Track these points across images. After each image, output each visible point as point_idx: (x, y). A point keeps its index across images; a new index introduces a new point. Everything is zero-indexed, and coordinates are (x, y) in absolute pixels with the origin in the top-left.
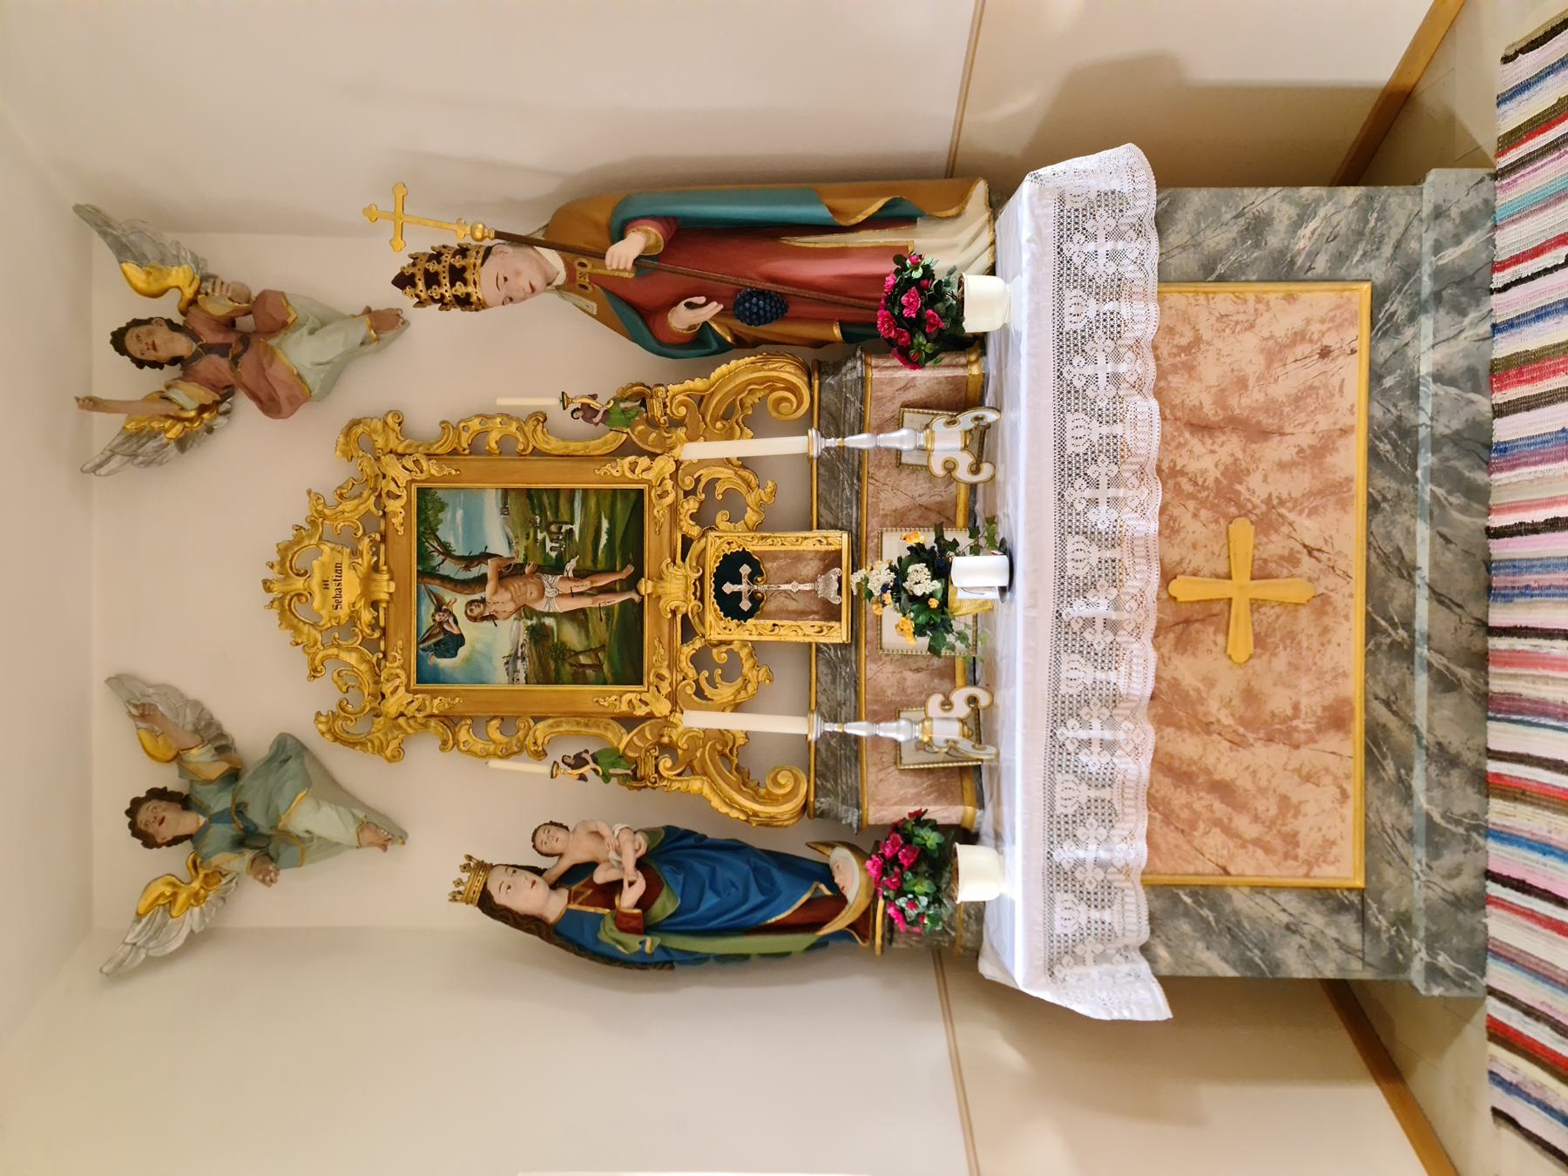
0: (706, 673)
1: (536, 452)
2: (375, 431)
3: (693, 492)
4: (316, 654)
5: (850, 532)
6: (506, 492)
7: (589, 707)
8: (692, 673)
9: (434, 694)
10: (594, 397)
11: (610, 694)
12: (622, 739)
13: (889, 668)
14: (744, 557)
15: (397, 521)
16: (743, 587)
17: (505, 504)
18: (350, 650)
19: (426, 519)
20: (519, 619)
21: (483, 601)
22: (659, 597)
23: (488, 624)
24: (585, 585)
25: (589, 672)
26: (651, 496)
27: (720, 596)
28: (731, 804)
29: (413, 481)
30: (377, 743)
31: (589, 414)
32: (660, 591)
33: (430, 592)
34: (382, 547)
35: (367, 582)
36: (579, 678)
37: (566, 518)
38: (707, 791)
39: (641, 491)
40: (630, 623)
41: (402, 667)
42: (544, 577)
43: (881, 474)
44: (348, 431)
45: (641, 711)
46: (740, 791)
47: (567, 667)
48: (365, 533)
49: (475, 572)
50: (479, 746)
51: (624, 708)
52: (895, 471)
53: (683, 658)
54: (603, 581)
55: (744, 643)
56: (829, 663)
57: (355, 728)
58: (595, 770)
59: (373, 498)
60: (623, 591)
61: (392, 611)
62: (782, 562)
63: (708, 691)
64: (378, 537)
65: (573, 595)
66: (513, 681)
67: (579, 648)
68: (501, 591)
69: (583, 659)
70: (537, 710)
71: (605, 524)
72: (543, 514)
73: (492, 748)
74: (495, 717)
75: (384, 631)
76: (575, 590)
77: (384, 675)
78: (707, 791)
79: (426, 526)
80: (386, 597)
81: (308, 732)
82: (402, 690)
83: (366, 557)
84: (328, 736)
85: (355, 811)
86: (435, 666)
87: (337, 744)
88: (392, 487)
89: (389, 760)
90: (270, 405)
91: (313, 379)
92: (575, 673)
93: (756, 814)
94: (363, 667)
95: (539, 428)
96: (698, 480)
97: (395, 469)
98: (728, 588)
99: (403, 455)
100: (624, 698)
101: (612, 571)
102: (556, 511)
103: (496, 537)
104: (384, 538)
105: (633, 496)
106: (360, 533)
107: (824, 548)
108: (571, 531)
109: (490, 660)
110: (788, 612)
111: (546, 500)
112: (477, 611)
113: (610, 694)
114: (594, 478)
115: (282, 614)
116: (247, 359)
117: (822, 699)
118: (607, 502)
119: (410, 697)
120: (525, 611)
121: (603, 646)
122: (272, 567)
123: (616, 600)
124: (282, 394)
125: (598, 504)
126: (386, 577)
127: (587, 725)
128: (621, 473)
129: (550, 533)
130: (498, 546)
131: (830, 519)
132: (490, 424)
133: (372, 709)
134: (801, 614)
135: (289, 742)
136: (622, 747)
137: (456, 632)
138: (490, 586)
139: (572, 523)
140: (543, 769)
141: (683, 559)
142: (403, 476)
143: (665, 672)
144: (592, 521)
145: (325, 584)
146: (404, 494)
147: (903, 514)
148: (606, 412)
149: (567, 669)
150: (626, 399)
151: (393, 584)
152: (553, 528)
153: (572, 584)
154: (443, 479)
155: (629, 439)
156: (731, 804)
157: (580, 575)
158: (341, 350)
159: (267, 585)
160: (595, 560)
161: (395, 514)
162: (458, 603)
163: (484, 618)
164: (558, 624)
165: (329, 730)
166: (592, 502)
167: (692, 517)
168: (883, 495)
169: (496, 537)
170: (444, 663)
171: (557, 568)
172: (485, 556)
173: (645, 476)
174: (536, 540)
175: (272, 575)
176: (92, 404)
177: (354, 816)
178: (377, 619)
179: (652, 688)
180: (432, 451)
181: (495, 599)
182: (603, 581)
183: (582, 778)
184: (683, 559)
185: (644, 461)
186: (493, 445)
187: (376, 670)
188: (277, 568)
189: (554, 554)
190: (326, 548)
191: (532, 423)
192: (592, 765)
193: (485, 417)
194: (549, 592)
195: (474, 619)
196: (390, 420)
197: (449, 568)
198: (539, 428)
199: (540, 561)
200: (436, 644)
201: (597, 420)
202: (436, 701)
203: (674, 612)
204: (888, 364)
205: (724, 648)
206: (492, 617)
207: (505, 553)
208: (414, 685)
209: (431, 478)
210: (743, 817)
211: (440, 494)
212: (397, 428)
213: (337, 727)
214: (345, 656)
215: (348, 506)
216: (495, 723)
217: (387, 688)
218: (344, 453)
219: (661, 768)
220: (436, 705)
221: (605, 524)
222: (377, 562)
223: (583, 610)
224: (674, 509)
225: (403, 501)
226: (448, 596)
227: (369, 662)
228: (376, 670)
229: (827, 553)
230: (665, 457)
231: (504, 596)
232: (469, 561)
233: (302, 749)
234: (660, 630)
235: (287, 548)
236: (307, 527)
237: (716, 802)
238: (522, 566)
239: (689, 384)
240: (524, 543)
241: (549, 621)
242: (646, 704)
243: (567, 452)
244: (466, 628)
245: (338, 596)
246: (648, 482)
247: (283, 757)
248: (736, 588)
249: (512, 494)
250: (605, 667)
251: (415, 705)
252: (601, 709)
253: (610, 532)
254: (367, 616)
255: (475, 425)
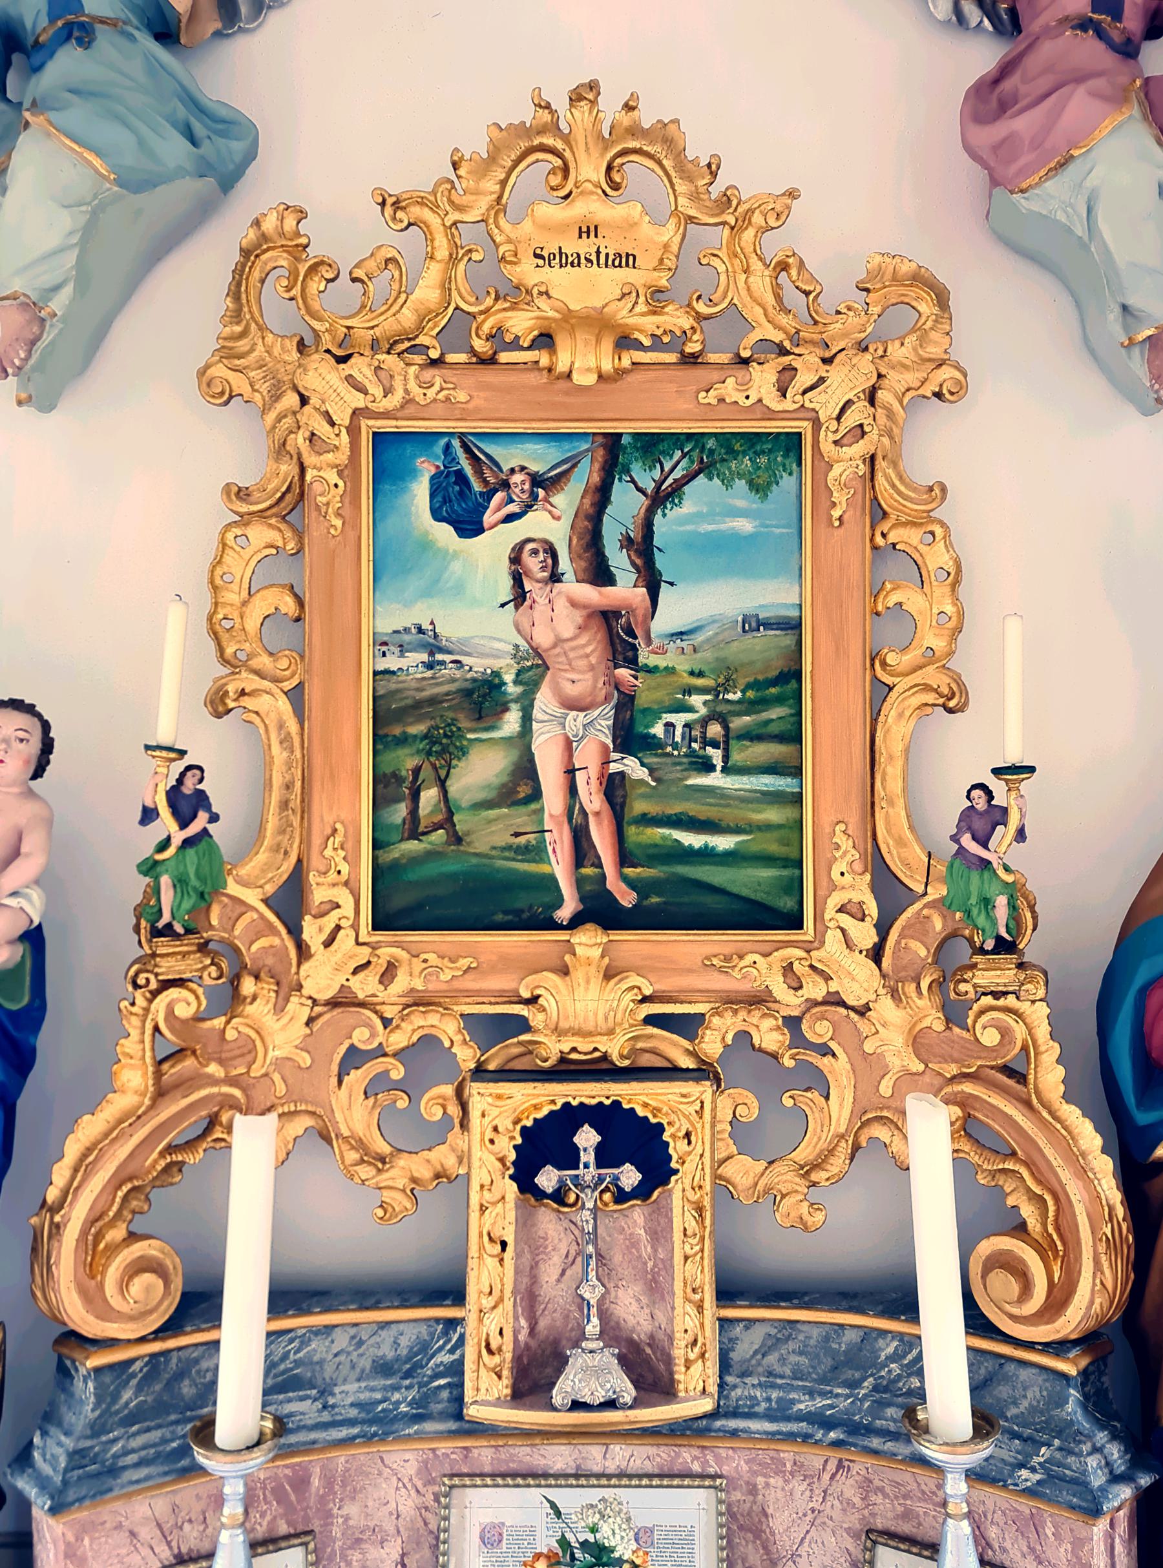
0: (397, 1073)
1: (881, 692)
2: (923, 340)
3: (798, 1040)
4: (434, 207)
5: (713, 1415)
6: (794, 626)
7: (324, 813)
8: (399, 1040)
9: (349, 471)
10: (1021, 835)
11: (352, 860)
12: (249, 887)
13: (407, 1504)
14: (658, 1172)
15: (730, 389)
16: (589, 1174)
17: (767, 625)
18: (446, 287)
19: (732, 453)
20: (516, 654)
21: (555, 577)
22: (565, 971)
23: (504, 588)
24: (592, 799)
25: (400, 811)
26: (785, 947)
27: (570, 1118)
28: (84, 1166)
29: (817, 424)
30: (243, 345)
31: (979, 825)
32: (578, 975)
33: (574, 462)
34: (672, 358)
35: (597, 323)
36: (385, 787)
37: (736, 757)
38: (117, 1105)
39: (795, 922)
40: (502, 901)
41: (408, 401)
42: (609, 710)
43: (848, 1487)
44: (922, 280)
45: (312, 932)
46: (117, 1182)
47: (411, 763)
48: (700, 318)
49: (619, 560)
50: (238, 567)
51: (319, 895)
52: (853, 1520)
53: (433, 1019)
54: (601, 837)
55: (463, 1158)
56: (424, 1348)
57: (273, 303)
58: (164, 845)
59: (777, 336)
60: (580, 882)
61: (533, 378)
62: (646, 1250)
63: (357, 1078)
64: (692, 348)
65: (571, 772)
66: (381, 644)
67: (455, 787)
68: (578, 617)
69: (429, 796)
70: (314, 695)
71: (723, 843)
72: (751, 706)
73: (232, 597)
74: (300, 603)
75: (489, 361)
76: (580, 777)
77: (391, 361)
78: (117, 1105)
79: (713, 454)
80: (562, 366)
81: (258, 199)
82: (359, 401)
83: (651, 323)
84: (252, 234)
85: (67, 291)
86: (413, 473)
87: (237, 257)
88: (805, 379)
89: (202, 373)
90: (990, 99)
91: (1053, 197)
92: (397, 778)
93: (57, 1228)
94: (408, 317)
95: (930, 698)
96: (825, 1050)
97: (845, 382)
98: (587, 1138)
99: (872, 401)
100: (342, 888)
101: (624, 858)
102: (753, 736)
103: (695, 607)
104: (691, 360)
105: (786, 903)
106: (701, 307)
107: (679, 1352)
108: (709, 767)
109: (429, 592)
110: (534, 1266)
111: (775, 713)
112: (533, 564)
113: (352, 860)
114: (826, 820)
115: (522, 130)
116: (1089, 51)
117: (341, 1340)
118: (774, 848)
119: (342, 417)
120: (535, 668)
121: (459, 840)
122: (629, 107)
123: (559, 865)
124: (1022, 124)
125: (767, 827)
126: (607, 366)
127: (284, 805)
128: (837, 883)
129: (705, 722)
130: (676, 609)
131: (743, 1351)
132: (941, 591)
133: (317, 335)
134: (529, 1299)
135: (238, 147)
136: (232, 888)
137: (488, 518)
138: (589, 593)
139: (726, 770)
140: (172, 716)
141: (650, 1020)
142: (826, 403)
143: (401, 983)
144: (729, 815)
145: (587, 231)
146: (788, 405)
147: (757, 1533)
148: (985, 864)
149: (406, 761)
150: (1013, 907)
151: (591, 379)
152: (715, 730)
153: (594, 771)
154: (822, 489)
155: (913, 897)
156: (84, 1166)
157: (615, 788)
158: (1121, 258)
159: (585, 94)
160: (647, 820)
161: (744, 385)
162: (553, 523)
163: (518, 580)
164: (507, 740)
165: (264, 238)
166: (773, 815)
167: (743, 1036)
168: (799, 1487)
169: (695, 607)
170: (420, 492)
171: (628, 737)
172: (652, 582)
173: (833, 938)
174: (689, 691)
175: (610, 106)
176: (503, 605)
177: (56, 288)
178: (515, 345)
179: (364, 954)
180: (880, 464)
181: (561, 605)
182: (601, 837)
183: (149, 815)
184: (650, 1020)
185: (865, 935)
186: (893, 600)
187: (402, 344)
188: (626, 119)
189: (658, 730)
190: (669, 233)
191: (942, 682)
192: (178, 837)
193: (955, 579)
194: (575, 721)
195: (516, 559)
196: (946, 373)
197: (626, 504)
198: (930, 698)
199: (642, 700)
200: (461, 477)
201: (967, 841)
202: (332, 477)
203: (533, 1000)
204: (1119, 1548)
205: (454, 1110)
206: (520, 597)
207: (661, 624)
208: (368, 426)
209: (823, 465)
210: (52, 1195)
211: (788, 482)
212: (928, 390)
213: (278, 255)
214: (434, 273)
215: (761, 282)
216: (289, 605)
217: (359, 368)
218: (876, 273)
219: (173, 993)
220: (324, 476)
221: (723, 843)
222: (639, 346)
223: (536, 794)
224: (759, 1000)
225: (772, 401)
226: (568, 500)
227: (420, 329)
228: (402, 344)
229: (669, 1361)
230: (877, 982)
231: (567, 622)
232: (643, 548)
233: (228, 181)
234: (493, 970)
235: (669, 142)
236: (716, 190)
237: (90, 1128)
238: (632, 662)
239: (1050, 1052)
240: (683, 665)
241: (511, 722)
242: (328, 943)
243: (881, 759)
244: (492, 547)
245: (563, 259)
246: (820, 940)
247: (199, 129)
248: (588, 1157)
249: (788, 640)
250: (412, 846)
251: (323, 429)
252: (317, 841)
253: (706, 855)
254: (521, 324)
255: (937, 558)
